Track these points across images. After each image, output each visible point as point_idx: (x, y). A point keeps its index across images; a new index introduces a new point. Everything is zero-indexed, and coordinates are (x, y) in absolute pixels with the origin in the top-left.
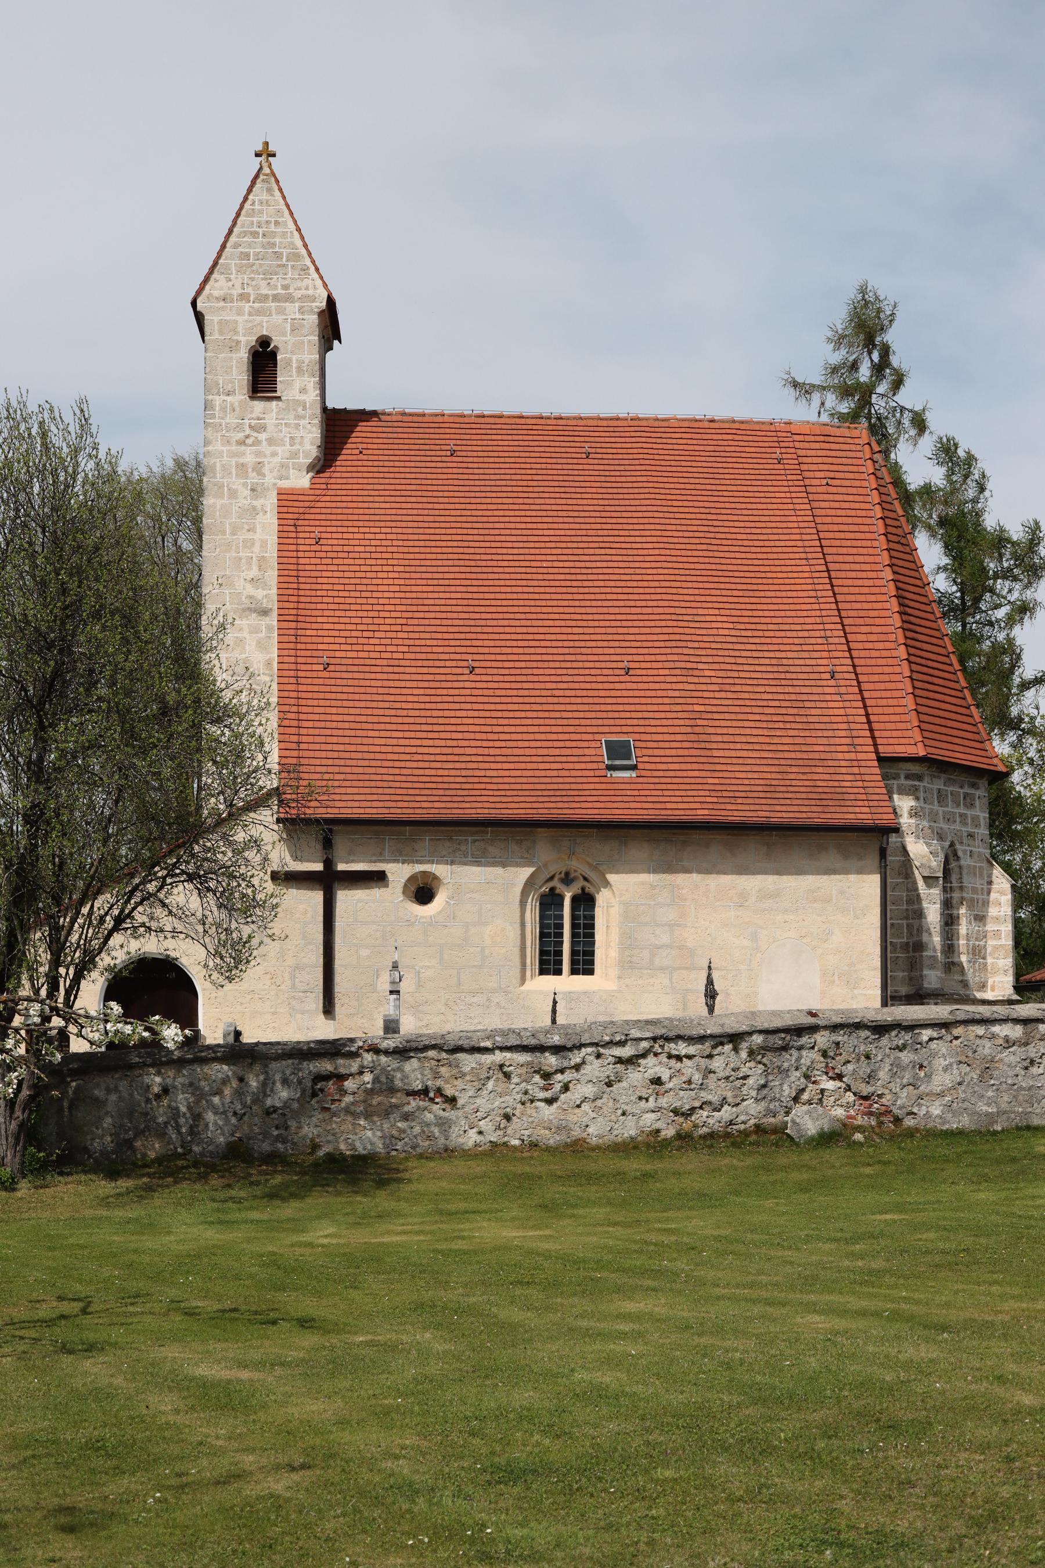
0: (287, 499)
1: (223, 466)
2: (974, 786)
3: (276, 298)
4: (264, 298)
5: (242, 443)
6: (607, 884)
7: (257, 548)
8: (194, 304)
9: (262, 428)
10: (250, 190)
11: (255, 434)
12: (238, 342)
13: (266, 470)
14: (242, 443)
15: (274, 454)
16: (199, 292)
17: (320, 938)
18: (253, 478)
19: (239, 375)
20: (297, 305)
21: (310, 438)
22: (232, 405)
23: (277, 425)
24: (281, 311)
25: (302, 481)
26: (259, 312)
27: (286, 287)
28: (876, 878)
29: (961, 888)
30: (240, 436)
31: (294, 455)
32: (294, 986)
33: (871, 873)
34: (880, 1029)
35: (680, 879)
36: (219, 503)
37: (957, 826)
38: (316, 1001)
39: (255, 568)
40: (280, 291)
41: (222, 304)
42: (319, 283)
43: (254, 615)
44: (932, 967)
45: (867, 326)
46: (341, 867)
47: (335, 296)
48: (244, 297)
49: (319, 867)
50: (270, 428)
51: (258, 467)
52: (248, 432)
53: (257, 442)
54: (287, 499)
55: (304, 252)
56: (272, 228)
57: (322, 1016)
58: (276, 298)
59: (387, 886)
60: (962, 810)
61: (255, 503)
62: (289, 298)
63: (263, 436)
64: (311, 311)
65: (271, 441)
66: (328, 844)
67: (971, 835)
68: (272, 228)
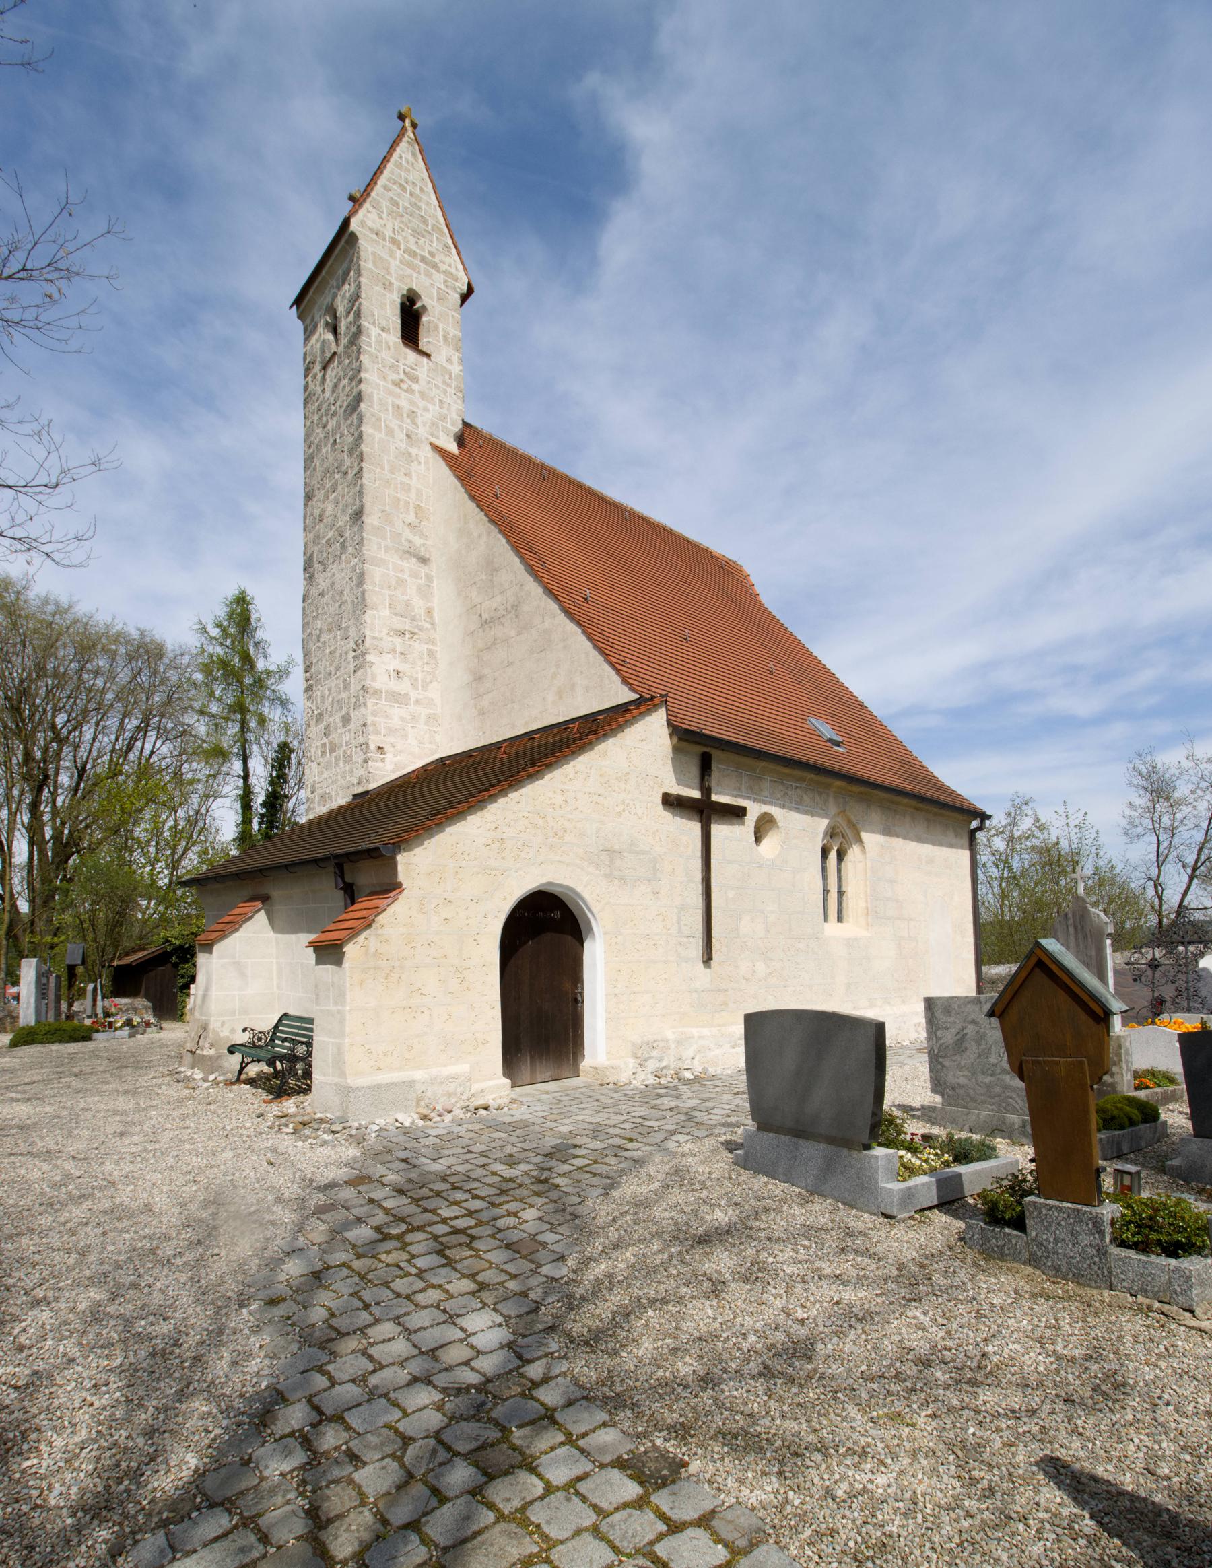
1: (380, 399)
4: (414, 254)
6: (860, 841)
7: (413, 495)
9: (416, 380)
10: (392, 148)
11: (409, 382)
13: (419, 420)
14: (397, 384)
15: (426, 410)
17: (698, 875)
18: (407, 425)
22: (387, 342)
23: (428, 383)
24: (429, 275)
26: (409, 265)
28: (967, 853)
31: (443, 418)
32: (680, 930)
33: (962, 848)
35: (898, 842)
36: (378, 435)
38: (696, 948)
39: (412, 514)
41: (375, 237)
43: (414, 560)
46: (714, 798)
49: (696, 794)
50: (422, 382)
52: (402, 376)
53: (410, 391)
57: (701, 965)
59: (743, 824)
61: (410, 450)
64: (454, 289)
66: (705, 766)
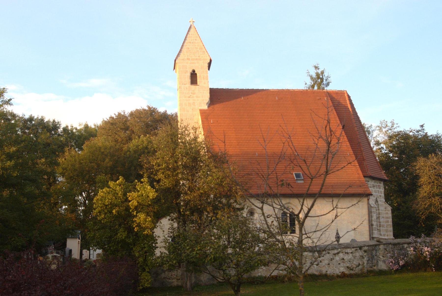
0: (202, 112)
2: (380, 183)
3: (196, 59)
4: (192, 60)
5: (189, 97)
8: (175, 61)
9: (194, 94)
12: (187, 71)
14: (189, 97)
16: (176, 58)
19: (188, 79)
20: (202, 61)
21: (207, 97)
25: (206, 107)
27: (199, 56)
29: (379, 210)
30: (189, 95)
34: (395, 245)
37: (377, 194)
40: (197, 57)
42: (208, 55)
44: (375, 230)
45: (209, 69)
47: (212, 59)
48: (188, 59)
51: (194, 103)
52: (191, 94)
53: (193, 97)
54: (202, 112)
55: (203, 47)
56: (195, 41)
57: (353, 238)
58: (196, 59)
60: (378, 189)
62: (200, 59)
63: (195, 95)
65: (197, 97)
67: (380, 196)
68: (195, 41)
